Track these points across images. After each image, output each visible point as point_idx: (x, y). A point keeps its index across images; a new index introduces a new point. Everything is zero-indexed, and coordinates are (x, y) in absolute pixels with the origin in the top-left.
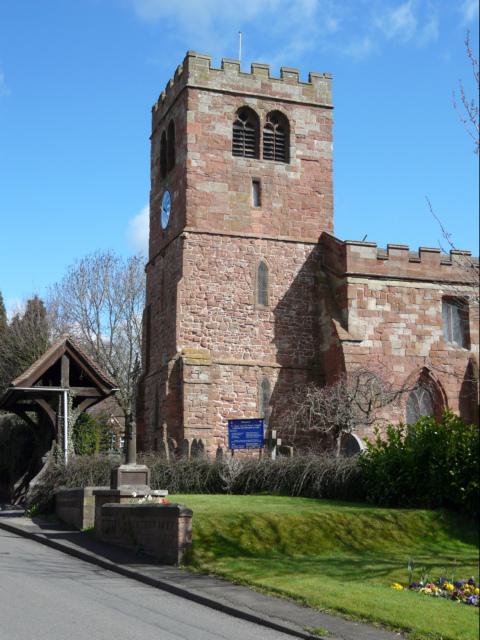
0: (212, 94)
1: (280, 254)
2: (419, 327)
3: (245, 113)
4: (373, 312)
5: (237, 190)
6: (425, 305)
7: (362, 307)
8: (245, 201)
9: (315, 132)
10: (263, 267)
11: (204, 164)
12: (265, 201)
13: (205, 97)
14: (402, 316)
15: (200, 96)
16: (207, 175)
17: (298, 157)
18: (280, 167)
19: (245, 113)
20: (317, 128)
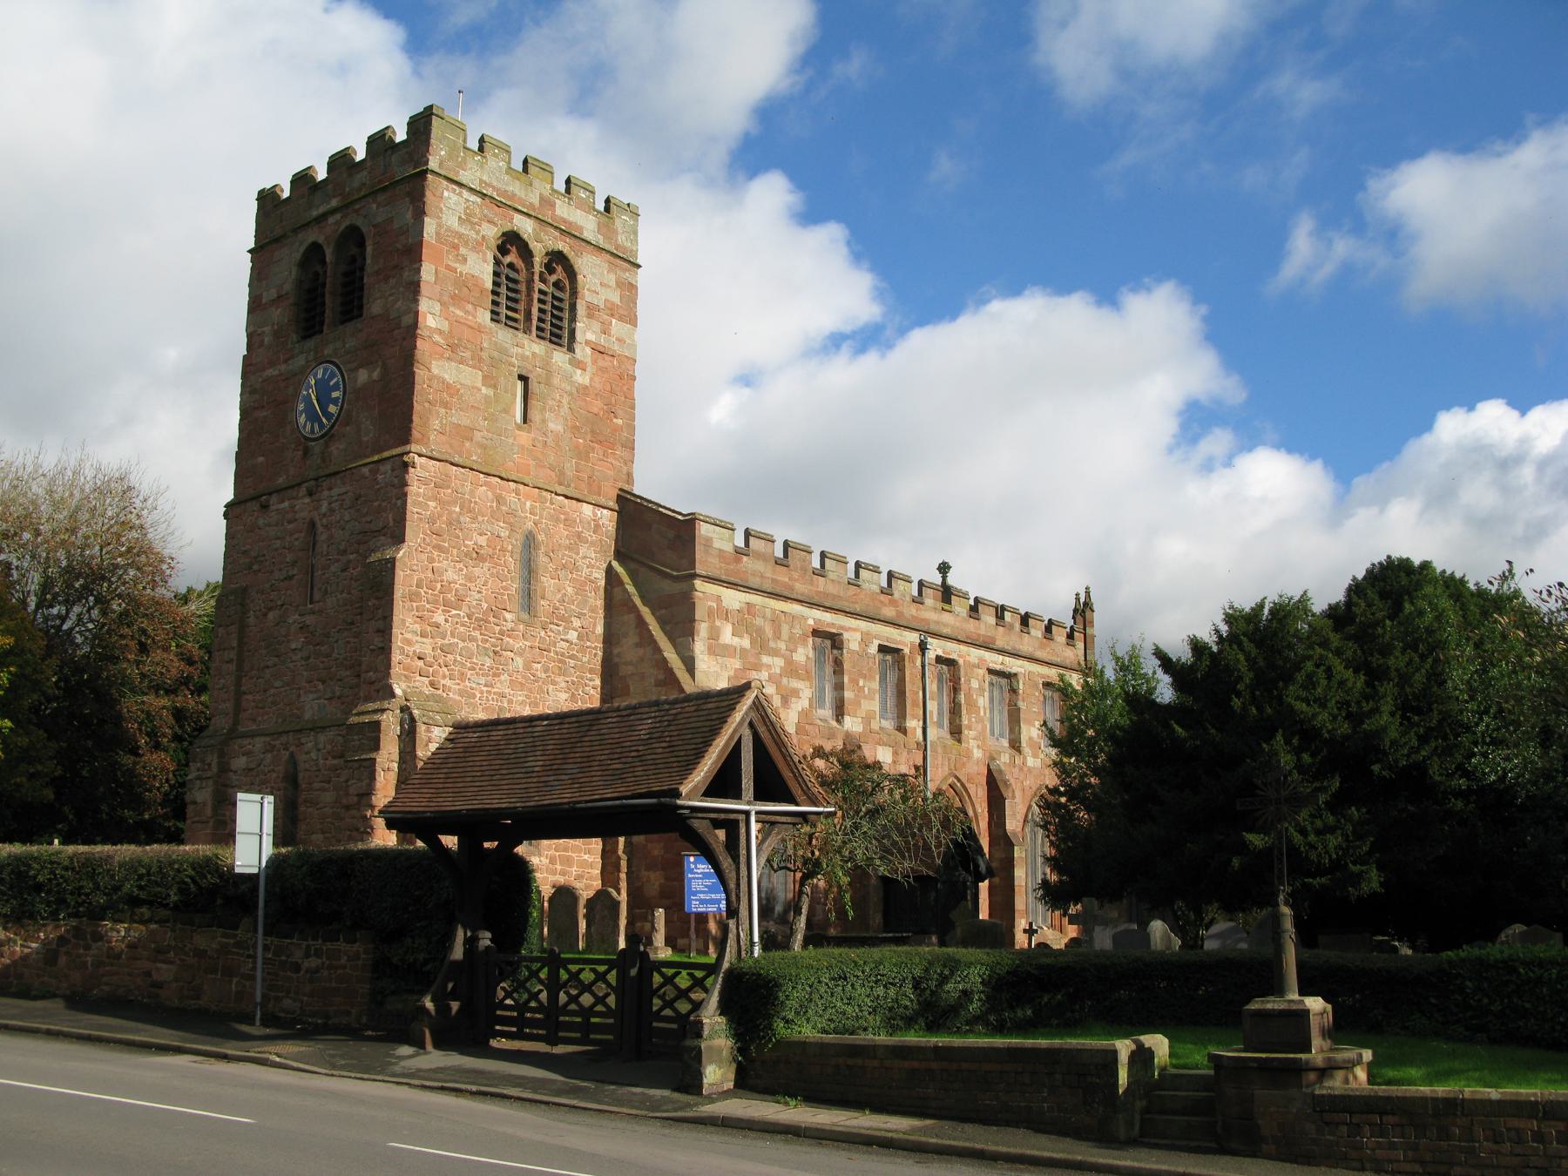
0: (466, 194)
1: (558, 520)
2: (785, 680)
3: (511, 241)
4: (726, 647)
5: (495, 387)
6: (793, 643)
7: (714, 634)
8: (506, 411)
9: (613, 304)
10: (530, 542)
11: (445, 326)
12: (534, 415)
13: (455, 198)
14: (765, 659)
15: (446, 194)
16: (453, 348)
17: (588, 343)
18: (559, 357)
19: (511, 241)
20: (615, 298)
